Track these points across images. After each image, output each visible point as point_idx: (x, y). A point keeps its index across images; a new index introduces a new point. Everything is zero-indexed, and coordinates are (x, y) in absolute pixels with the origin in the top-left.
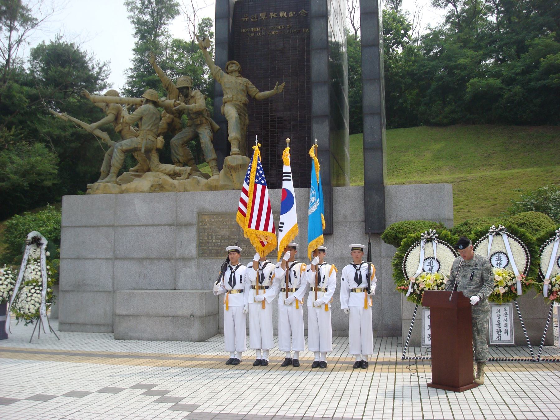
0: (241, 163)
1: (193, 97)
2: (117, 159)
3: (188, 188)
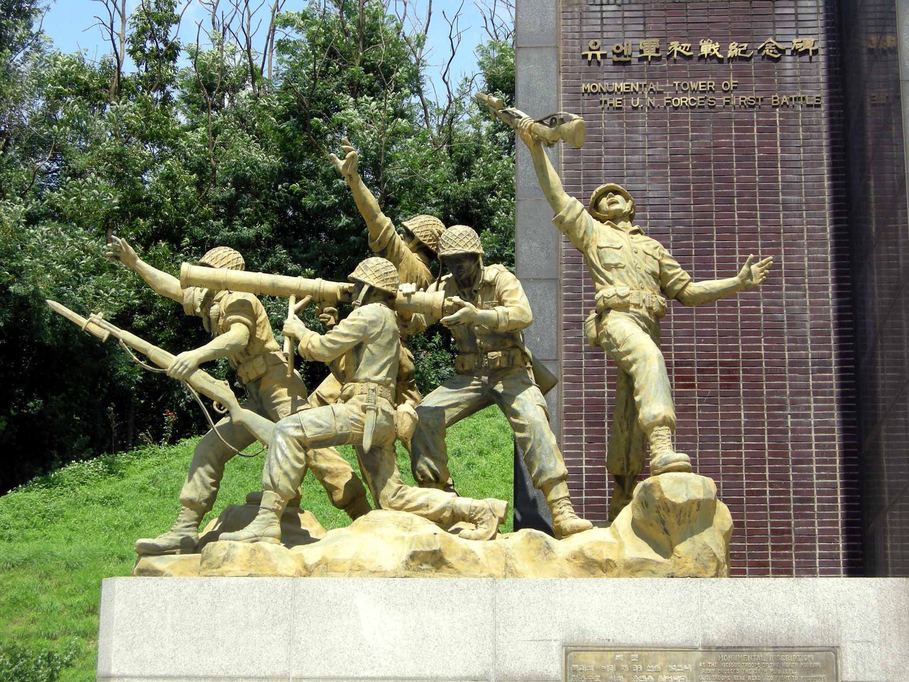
0: (701, 496)
1: (491, 285)
2: (287, 467)
3: (519, 567)
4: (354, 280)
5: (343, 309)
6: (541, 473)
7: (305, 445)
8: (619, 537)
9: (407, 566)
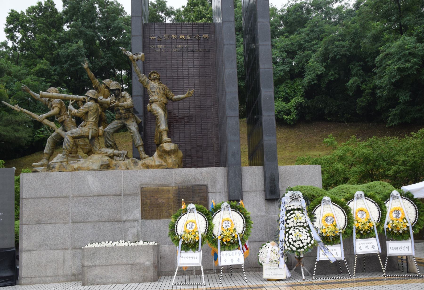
1: (123, 97)
4: (86, 96)
5: (84, 102)
6: (136, 144)
7: (74, 138)
8: (155, 159)
9: (100, 168)
